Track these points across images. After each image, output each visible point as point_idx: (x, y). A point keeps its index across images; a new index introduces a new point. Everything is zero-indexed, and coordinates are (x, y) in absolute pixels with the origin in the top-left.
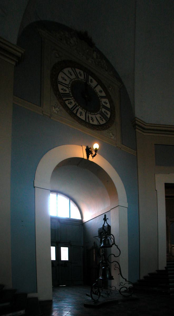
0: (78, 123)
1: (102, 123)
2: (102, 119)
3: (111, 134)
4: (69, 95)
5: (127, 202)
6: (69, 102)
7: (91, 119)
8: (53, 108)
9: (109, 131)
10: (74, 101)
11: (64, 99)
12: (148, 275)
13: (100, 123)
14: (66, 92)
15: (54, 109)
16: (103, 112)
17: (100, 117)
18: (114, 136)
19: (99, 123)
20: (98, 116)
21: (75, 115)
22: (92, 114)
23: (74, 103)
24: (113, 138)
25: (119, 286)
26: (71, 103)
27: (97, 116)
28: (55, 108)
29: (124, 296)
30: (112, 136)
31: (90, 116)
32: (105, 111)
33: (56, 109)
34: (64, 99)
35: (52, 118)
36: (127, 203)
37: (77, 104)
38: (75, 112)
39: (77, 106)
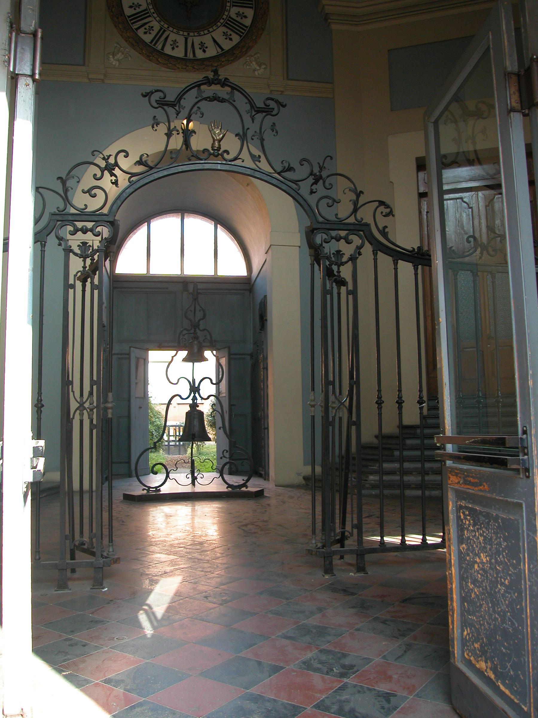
0: (164, 69)
1: (227, 45)
2: (231, 35)
3: (254, 65)
4: (148, 13)
5: (297, 231)
6: (145, 29)
7: (200, 46)
8: (111, 57)
9: (248, 58)
10: (159, 22)
11: (135, 27)
12: (375, 441)
13: (222, 49)
14: (142, 8)
15: (112, 59)
16: (234, 16)
17: (225, 34)
18: (263, 67)
19: (219, 50)
20: (218, 33)
21: (161, 53)
22: (202, 33)
23: (156, 26)
24: (260, 71)
25: (221, 458)
26: (174, 45)
27: (214, 34)
28: (114, 55)
29: (229, 486)
30: (258, 68)
31: (197, 40)
32: (238, 14)
33: (116, 58)
34: (135, 27)
35: (107, 81)
36: (299, 234)
37: (166, 26)
38: (159, 47)
39: (165, 31)
